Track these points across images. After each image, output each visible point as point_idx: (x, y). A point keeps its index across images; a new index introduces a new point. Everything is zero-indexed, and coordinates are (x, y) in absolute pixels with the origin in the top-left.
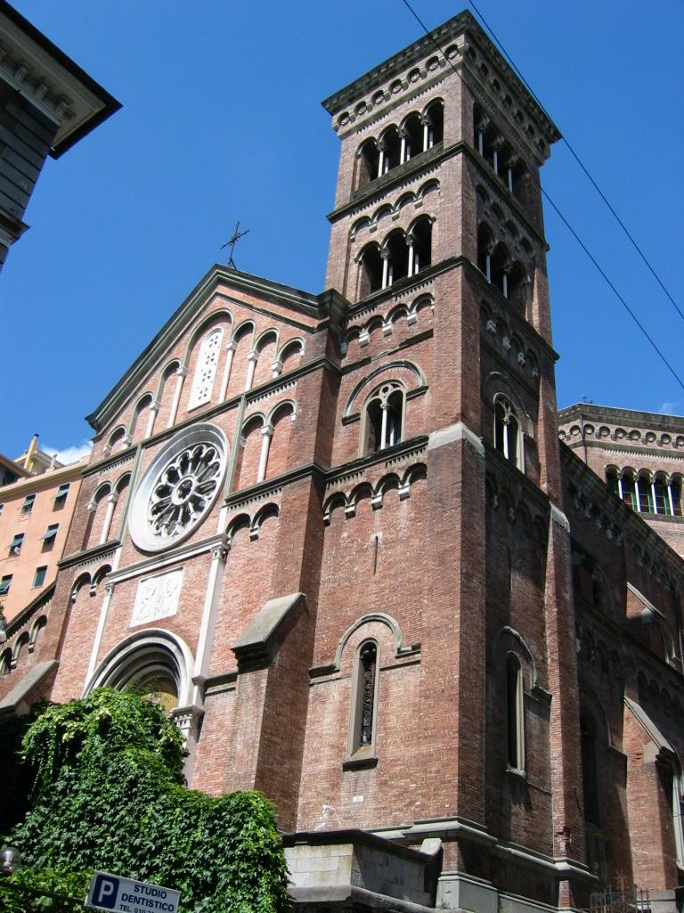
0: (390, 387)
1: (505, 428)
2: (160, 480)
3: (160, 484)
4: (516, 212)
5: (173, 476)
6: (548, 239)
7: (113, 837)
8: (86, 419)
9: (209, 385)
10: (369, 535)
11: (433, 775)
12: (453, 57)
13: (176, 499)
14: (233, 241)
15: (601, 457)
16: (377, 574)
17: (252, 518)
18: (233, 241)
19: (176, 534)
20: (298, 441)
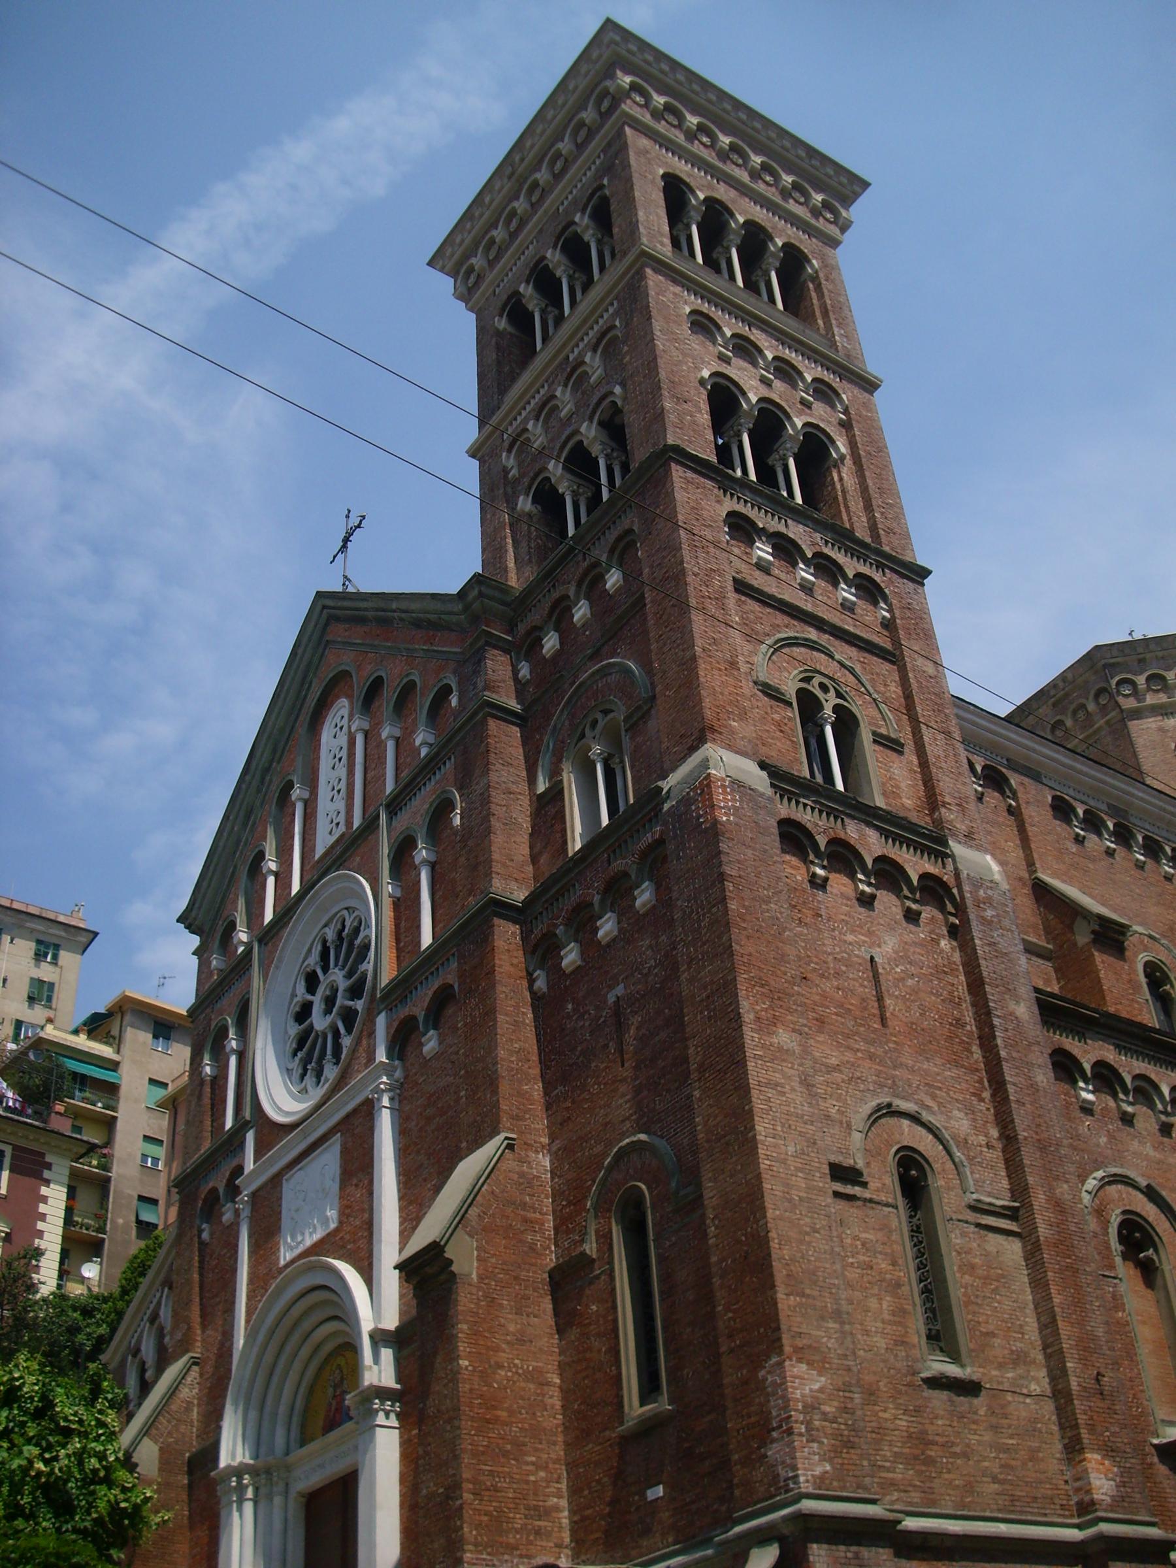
0: (599, 716)
1: (828, 730)
2: (294, 995)
3: (296, 1000)
4: (782, 337)
5: (312, 981)
6: (873, 366)
7: (1155, 1464)
8: (178, 921)
9: (341, 805)
10: (605, 996)
11: (753, 1419)
12: (635, 102)
13: (319, 1021)
14: (344, 546)
15: (1161, 730)
16: (626, 1065)
17: (421, 1019)
18: (344, 546)
19: (327, 1080)
20: (468, 859)
